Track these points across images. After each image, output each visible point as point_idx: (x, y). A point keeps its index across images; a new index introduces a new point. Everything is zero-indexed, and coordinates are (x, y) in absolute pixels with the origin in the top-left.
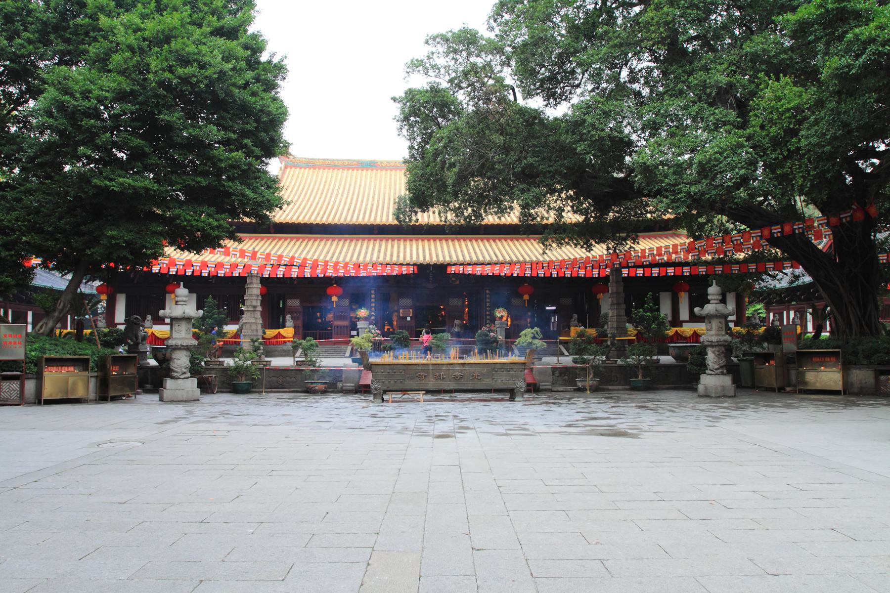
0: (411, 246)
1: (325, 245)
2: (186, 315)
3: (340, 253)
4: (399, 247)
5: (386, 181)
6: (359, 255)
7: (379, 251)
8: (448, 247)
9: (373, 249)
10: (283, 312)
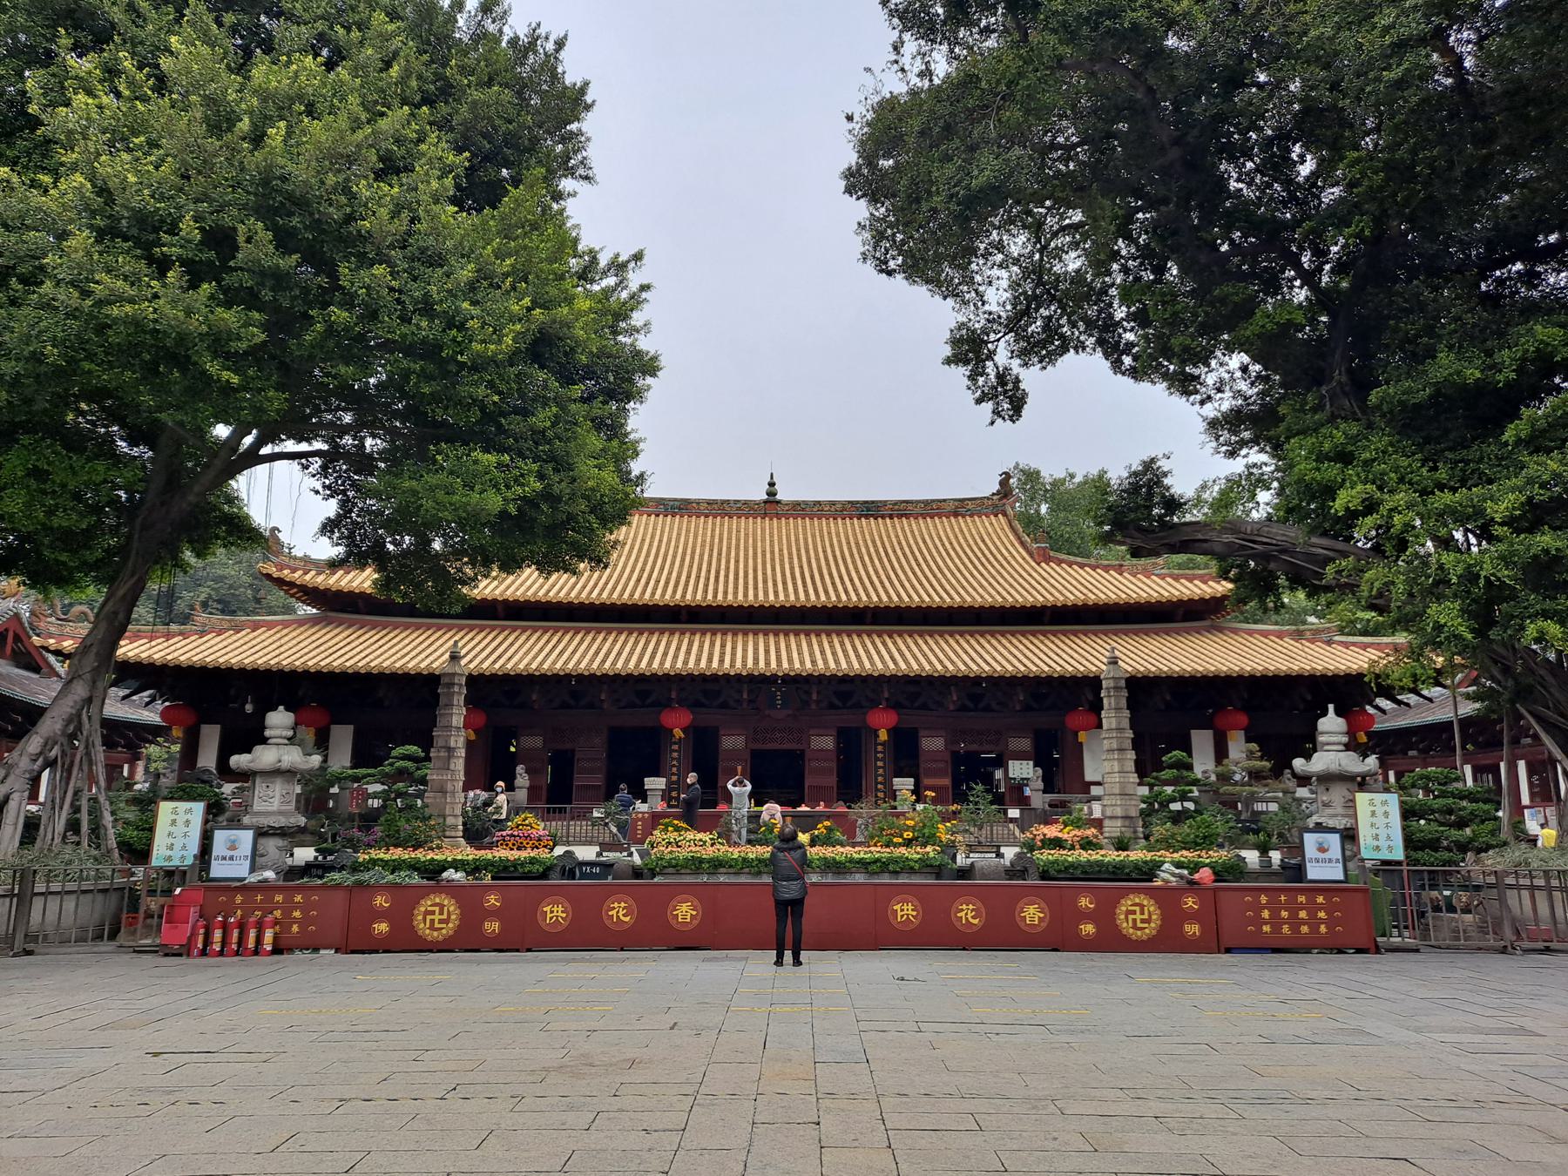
0: (788, 524)
2: (285, 765)
4: (723, 646)
5: (704, 535)
7: (688, 652)
8: (810, 645)
9: (678, 649)
10: (513, 760)
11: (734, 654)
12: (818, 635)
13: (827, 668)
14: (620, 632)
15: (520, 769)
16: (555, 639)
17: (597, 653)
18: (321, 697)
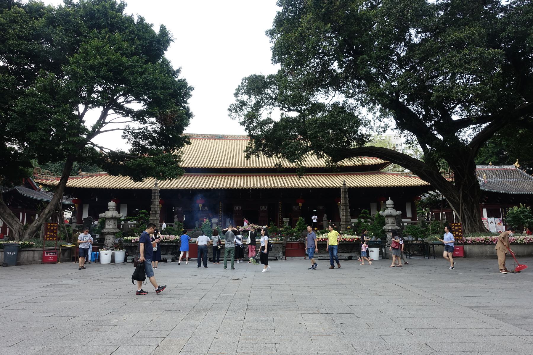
1: (196, 178)
2: (114, 216)
3: (204, 183)
4: (234, 180)
6: (213, 184)
8: (266, 179)
9: (221, 181)
10: (173, 214)
11: (237, 182)
12: (275, 176)
13: (264, 186)
14: (204, 176)
15: (175, 216)
16: (185, 178)
17: (197, 183)
18: (121, 196)
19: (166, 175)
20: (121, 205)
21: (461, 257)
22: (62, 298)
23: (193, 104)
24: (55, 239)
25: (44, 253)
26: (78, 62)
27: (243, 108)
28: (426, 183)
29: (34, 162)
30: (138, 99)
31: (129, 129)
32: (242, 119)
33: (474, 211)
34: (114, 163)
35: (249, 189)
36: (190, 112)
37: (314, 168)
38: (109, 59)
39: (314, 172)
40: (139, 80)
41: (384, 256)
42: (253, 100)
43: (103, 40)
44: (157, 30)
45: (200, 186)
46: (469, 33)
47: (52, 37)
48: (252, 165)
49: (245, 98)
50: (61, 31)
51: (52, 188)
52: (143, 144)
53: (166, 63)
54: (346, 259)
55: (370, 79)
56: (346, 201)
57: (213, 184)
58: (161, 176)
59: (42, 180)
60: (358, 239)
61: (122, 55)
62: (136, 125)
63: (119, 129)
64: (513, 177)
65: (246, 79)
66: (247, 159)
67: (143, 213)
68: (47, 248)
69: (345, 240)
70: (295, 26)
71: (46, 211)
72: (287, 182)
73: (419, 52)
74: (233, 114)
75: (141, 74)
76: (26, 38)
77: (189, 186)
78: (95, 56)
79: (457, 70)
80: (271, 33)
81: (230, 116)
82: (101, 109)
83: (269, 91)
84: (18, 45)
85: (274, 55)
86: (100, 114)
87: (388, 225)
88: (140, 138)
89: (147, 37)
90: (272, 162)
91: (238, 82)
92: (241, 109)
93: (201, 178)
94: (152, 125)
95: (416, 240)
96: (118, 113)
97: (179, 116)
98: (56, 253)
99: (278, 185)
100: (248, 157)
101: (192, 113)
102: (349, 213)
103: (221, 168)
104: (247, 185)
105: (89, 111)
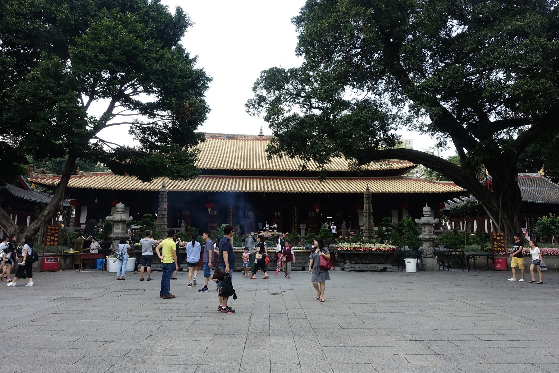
1: (205, 180)
2: (123, 219)
3: (213, 185)
4: (246, 183)
11: (250, 185)
14: (213, 178)
17: (206, 185)
18: (125, 196)
19: (182, 174)
20: (82, 207)
21: (504, 270)
22: (80, 315)
23: (210, 97)
24: (56, 243)
25: (44, 260)
26: (87, 44)
27: (262, 103)
28: (462, 189)
29: (30, 158)
30: (148, 91)
31: (138, 123)
32: (265, 114)
33: (515, 221)
34: (122, 161)
35: (263, 193)
36: (207, 106)
37: (344, 171)
38: (122, 41)
39: (337, 175)
40: (156, 66)
41: (420, 268)
42: (271, 96)
43: (114, 20)
44: (173, 12)
45: (202, 189)
46: (530, 22)
47: (56, 17)
48: (255, 167)
49: (264, 92)
50: (66, 9)
51: (48, 188)
52: (153, 140)
53: (180, 50)
54: (379, 271)
55: (401, 75)
56: (369, 207)
57: (224, 186)
58: (176, 175)
59: (36, 178)
60: (393, 249)
61: (137, 37)
62: (145, 119)
63: (127, 123)
64: (539, 185)
65: (265, 72)
66: (281, 159)
67: (147, 217)
68: (48, 254)
69: (379, 250)
70: (329, 11)
71: (46, 213)
72: (303, 186)
73: (471, 42)
74: (252, 110)
75: (158, 60)
76: (26, 17)
77: (191, 189)
78: (107, 38)
79: (516, 62)
80: (297, 21)
81: (248, 112)
82: (110, 100)
83: (291, 87)
84: (17, 23)
85: (300, 45)
86: (109, 104)
87: (425, 234)
88: (148, 134)
89: (163, 20)
90: (293, 163)
91: (257, 76)
92: (259, 105)
93: (210, 180)
94: (164, 119)
95: (455, 251)
96: (125, 106)
97: (197, 110)
98: (57, 259)
99: (294, 189)
100: (269, 157)
101: (208, 106)
102: (372, 221)
103: (231, 170)
104: (261, 189)
105: (94, 103)
